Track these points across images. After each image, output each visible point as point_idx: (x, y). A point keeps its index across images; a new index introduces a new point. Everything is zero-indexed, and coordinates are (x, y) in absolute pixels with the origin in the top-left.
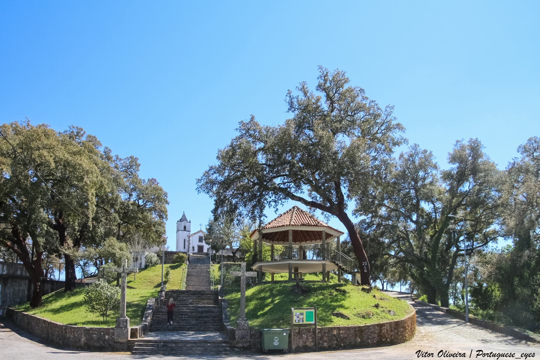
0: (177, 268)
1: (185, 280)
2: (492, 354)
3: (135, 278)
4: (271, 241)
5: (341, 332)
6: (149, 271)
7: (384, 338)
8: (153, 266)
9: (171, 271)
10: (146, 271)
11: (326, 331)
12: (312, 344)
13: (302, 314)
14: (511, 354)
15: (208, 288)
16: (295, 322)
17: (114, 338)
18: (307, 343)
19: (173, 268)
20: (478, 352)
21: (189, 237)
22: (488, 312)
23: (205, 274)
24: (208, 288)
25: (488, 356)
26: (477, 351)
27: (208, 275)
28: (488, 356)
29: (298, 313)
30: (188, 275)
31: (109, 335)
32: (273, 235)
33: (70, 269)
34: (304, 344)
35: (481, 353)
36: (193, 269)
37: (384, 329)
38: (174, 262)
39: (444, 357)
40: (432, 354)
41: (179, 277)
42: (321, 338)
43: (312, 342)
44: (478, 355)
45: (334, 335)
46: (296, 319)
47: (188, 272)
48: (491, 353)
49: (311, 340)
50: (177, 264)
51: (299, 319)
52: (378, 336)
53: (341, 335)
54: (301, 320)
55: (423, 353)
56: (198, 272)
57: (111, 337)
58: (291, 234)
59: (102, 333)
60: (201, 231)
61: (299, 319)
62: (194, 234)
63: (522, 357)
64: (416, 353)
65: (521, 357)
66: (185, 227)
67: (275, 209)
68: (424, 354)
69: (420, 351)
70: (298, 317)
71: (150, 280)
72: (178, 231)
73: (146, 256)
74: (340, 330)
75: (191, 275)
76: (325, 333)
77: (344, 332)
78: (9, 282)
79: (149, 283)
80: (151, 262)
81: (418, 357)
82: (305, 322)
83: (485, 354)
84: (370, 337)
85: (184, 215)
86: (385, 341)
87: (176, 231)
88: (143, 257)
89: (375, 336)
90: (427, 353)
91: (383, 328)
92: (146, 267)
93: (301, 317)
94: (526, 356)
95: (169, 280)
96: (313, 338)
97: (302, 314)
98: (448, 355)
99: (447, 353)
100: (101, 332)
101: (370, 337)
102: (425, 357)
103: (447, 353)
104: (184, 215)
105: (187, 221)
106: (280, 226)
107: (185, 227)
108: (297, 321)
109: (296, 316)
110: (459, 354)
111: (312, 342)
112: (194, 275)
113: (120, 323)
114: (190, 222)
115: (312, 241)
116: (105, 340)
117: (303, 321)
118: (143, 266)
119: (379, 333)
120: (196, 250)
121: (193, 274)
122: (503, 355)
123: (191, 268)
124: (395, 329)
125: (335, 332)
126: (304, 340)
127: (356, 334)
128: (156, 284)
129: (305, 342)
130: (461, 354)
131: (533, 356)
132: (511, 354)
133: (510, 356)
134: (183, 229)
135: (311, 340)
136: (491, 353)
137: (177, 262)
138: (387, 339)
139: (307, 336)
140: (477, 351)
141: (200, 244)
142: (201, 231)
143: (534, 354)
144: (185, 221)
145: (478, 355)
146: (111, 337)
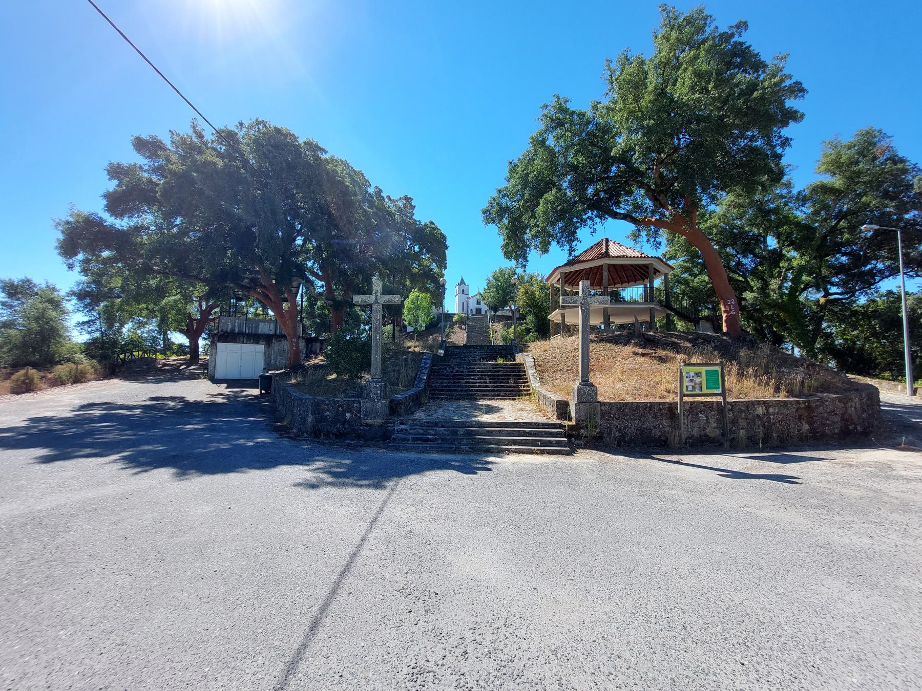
4: (571, 286)
5: (771, 410)
7: (851, 425)
11: (743, 408)
12: (718, 432)
13: (698, 375)
16: (687, 390)
17: (360, 417)
18: (708, 431)
22: (27, 371)
29: (692, 374)
31: (350, 412)
32: (572, 274)
33: (286, 300)
34: (702, 433)
37: (851, 406)
42: (734, 422)
43: (717, 428)
45: (758, 416)
46: (687, 384)
49: (715, 425)
51: (693, 384)
52: (843, 419)
53: (772, 417)
54: (697, 387)
57: (356, 415)
58: (605, 269)
59: (340, 409)
61: (693, 384)
62: (473, 297)
66: (463, 291)
67: (592, 230)
70: (692, 381)
74: (770, 406)
76: (741, 411)
77: (776, 410)
78: (273, 342)
82: (705, 391)
84: (828, 422)
85: (462, 279)
86: (853, 430)
89: (835, 420)
91: (850, 404)
93: (698, 380)
96: (718, 421)
97: (698, 375)
100: (339, 406)
101: (828, 422)
104: (462, 279)
106: (589, 260)
107: (463, 291)
108: (690, 388)
109: (687, 379)
111: (717, 428)
113: (371, 391)
115: (637, 282)
116: (345, 422)
117: (701, 387)
119: (843, 415)
120: (474, 312)
124: (868, 406)
125: (760, 410)
126: (702, 423)
127: (800, 416)
129: (704, 429)
135: (715, 425)
138: (856, 425)
139: (706, 417)
141: (478, 306)
146: (356, 415)
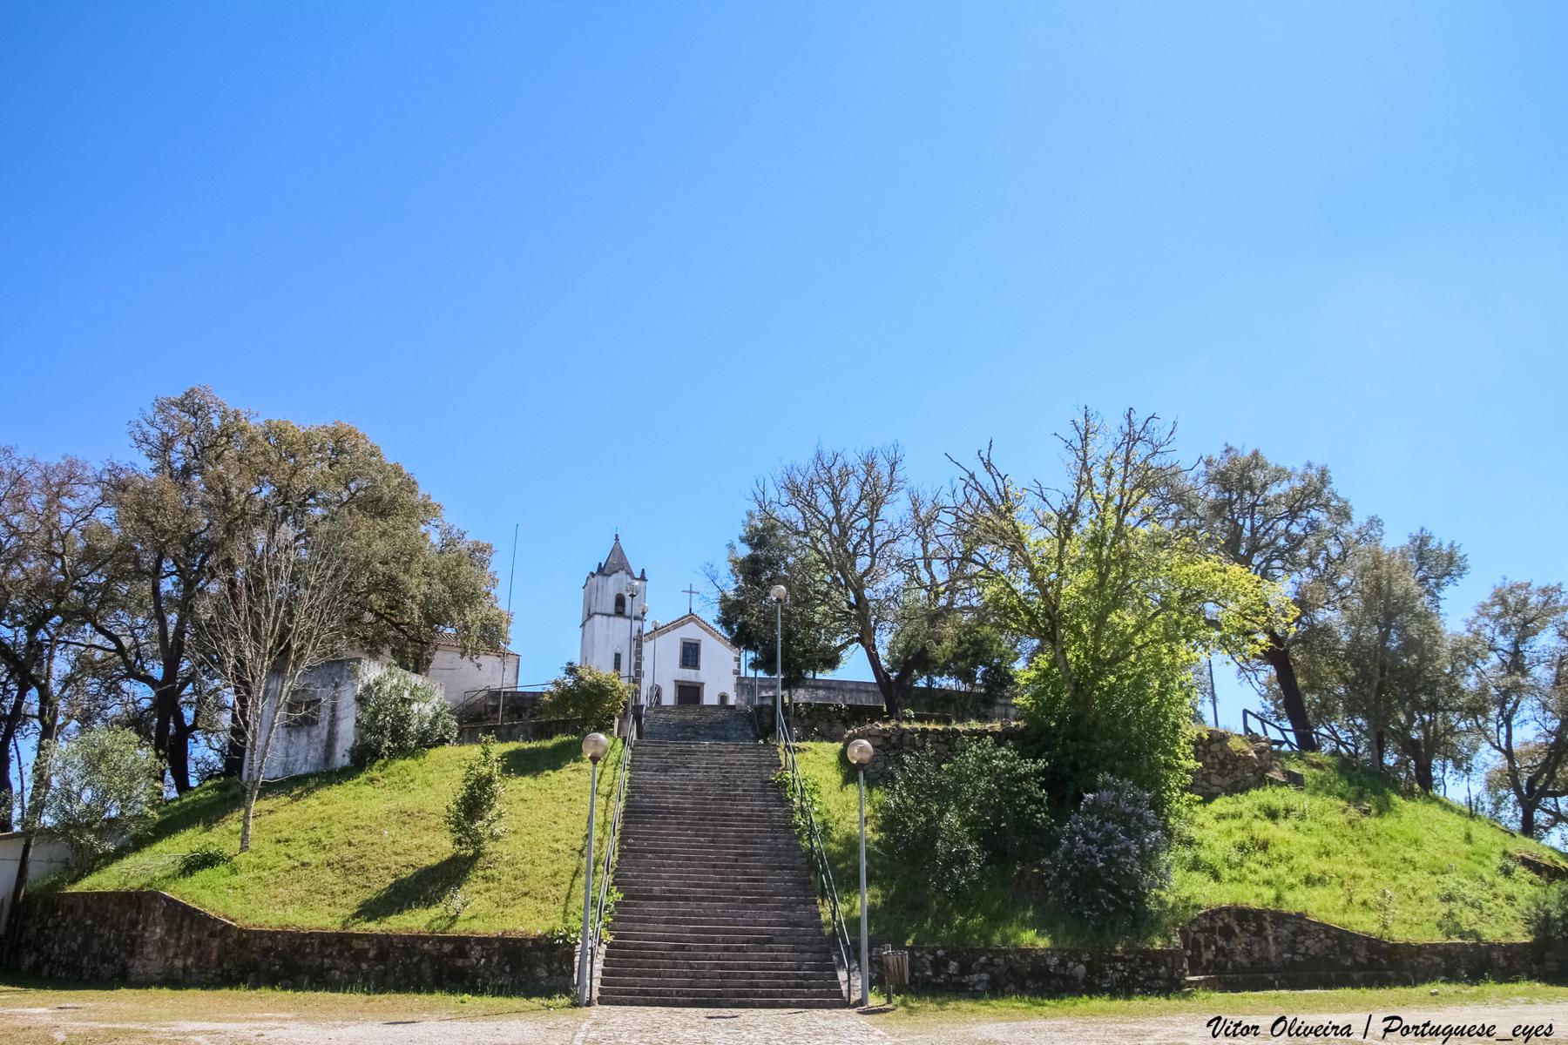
0: (556, 767)
1: (609, 848)
2: (1427, 1029)
3: (244, 839)
6: (368, 790)
8: (403, 752)
9: (514, 792)
10: (350, 784)
14: (1483, 1026)
15: (800, 913)
19: (520, 764)
20: (1390, 1022)
21: (638, 640)
23: (758, 805)
24: (800, 913)
25: (1416, 1035)
26: (1386, 1019)
27: (778, 812)
28: (1416, 1035)
30: (632, 813)
35: (1396, 1024)
36: (666, 770)
38: (543, 732)
39: (1290, 1035)
40: (1253, 1027)
41: (570, 829)
44: (1387, 1030)
47: (635, 788)
48: (1427, 1025)
50: (558, 739)
55: (1228, 1024)
56: (700, 788)
60: (691, 617)
63: (1515, 1035)
64: (1209, 1025)
65: (1512, 1037)
66: (620, 601)
68: (1232, 1028)
69: (1219, 1018)
71: (348, 853)
72: (590, 616)
73: (368, 688)
75: (655, 811)
79: (329, 877)
80: (398, 734)
81: (1215, 1036)
83: (1407, 1026)
85: (617, 552)
87: (578, 615)
88: (347, 698)
90: (1239, 1024)
92: (363, 758)
94: (1529, 1032)
95: (489, 846)
98: (1300, 1032)
99: (1298, 1024)
102: (1235, 1035)
103: (1298, 1024)
104: (617, 552)
105: (630, 573)
110: (1334, 1027)
112: (678, 811)
114: (643, 578)
118: (341, 758)
121: (670, 801)
122: (1460, 1032)
123: (656, 763)
128: (381, 882)
130: (1338, 1027)
131: (1547, 1035)
132: (1483, 1026)
133: (1480, 1035)
134: (611, 609)
136: (1426, 1025)
137: (563, 727)
140: (1386, 1019)
142: (691, 617)
143: (1551, 1027)
144: (622, 574)
145: (1387, 1030)
